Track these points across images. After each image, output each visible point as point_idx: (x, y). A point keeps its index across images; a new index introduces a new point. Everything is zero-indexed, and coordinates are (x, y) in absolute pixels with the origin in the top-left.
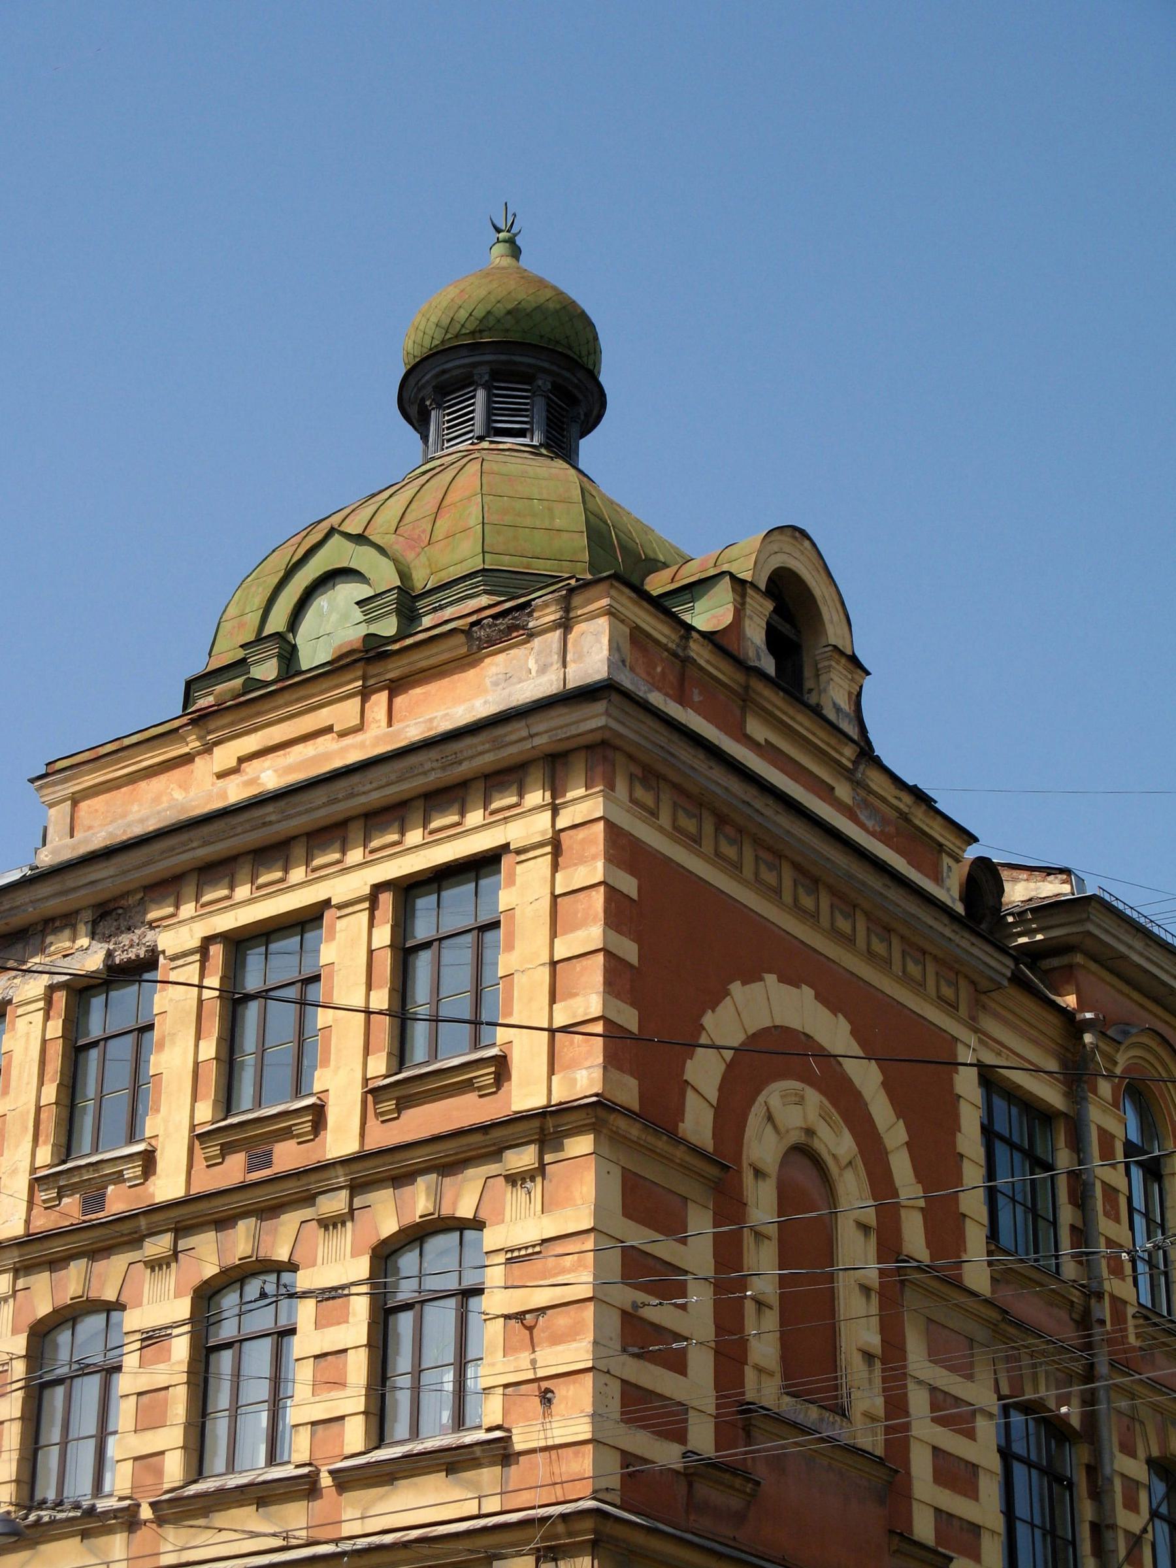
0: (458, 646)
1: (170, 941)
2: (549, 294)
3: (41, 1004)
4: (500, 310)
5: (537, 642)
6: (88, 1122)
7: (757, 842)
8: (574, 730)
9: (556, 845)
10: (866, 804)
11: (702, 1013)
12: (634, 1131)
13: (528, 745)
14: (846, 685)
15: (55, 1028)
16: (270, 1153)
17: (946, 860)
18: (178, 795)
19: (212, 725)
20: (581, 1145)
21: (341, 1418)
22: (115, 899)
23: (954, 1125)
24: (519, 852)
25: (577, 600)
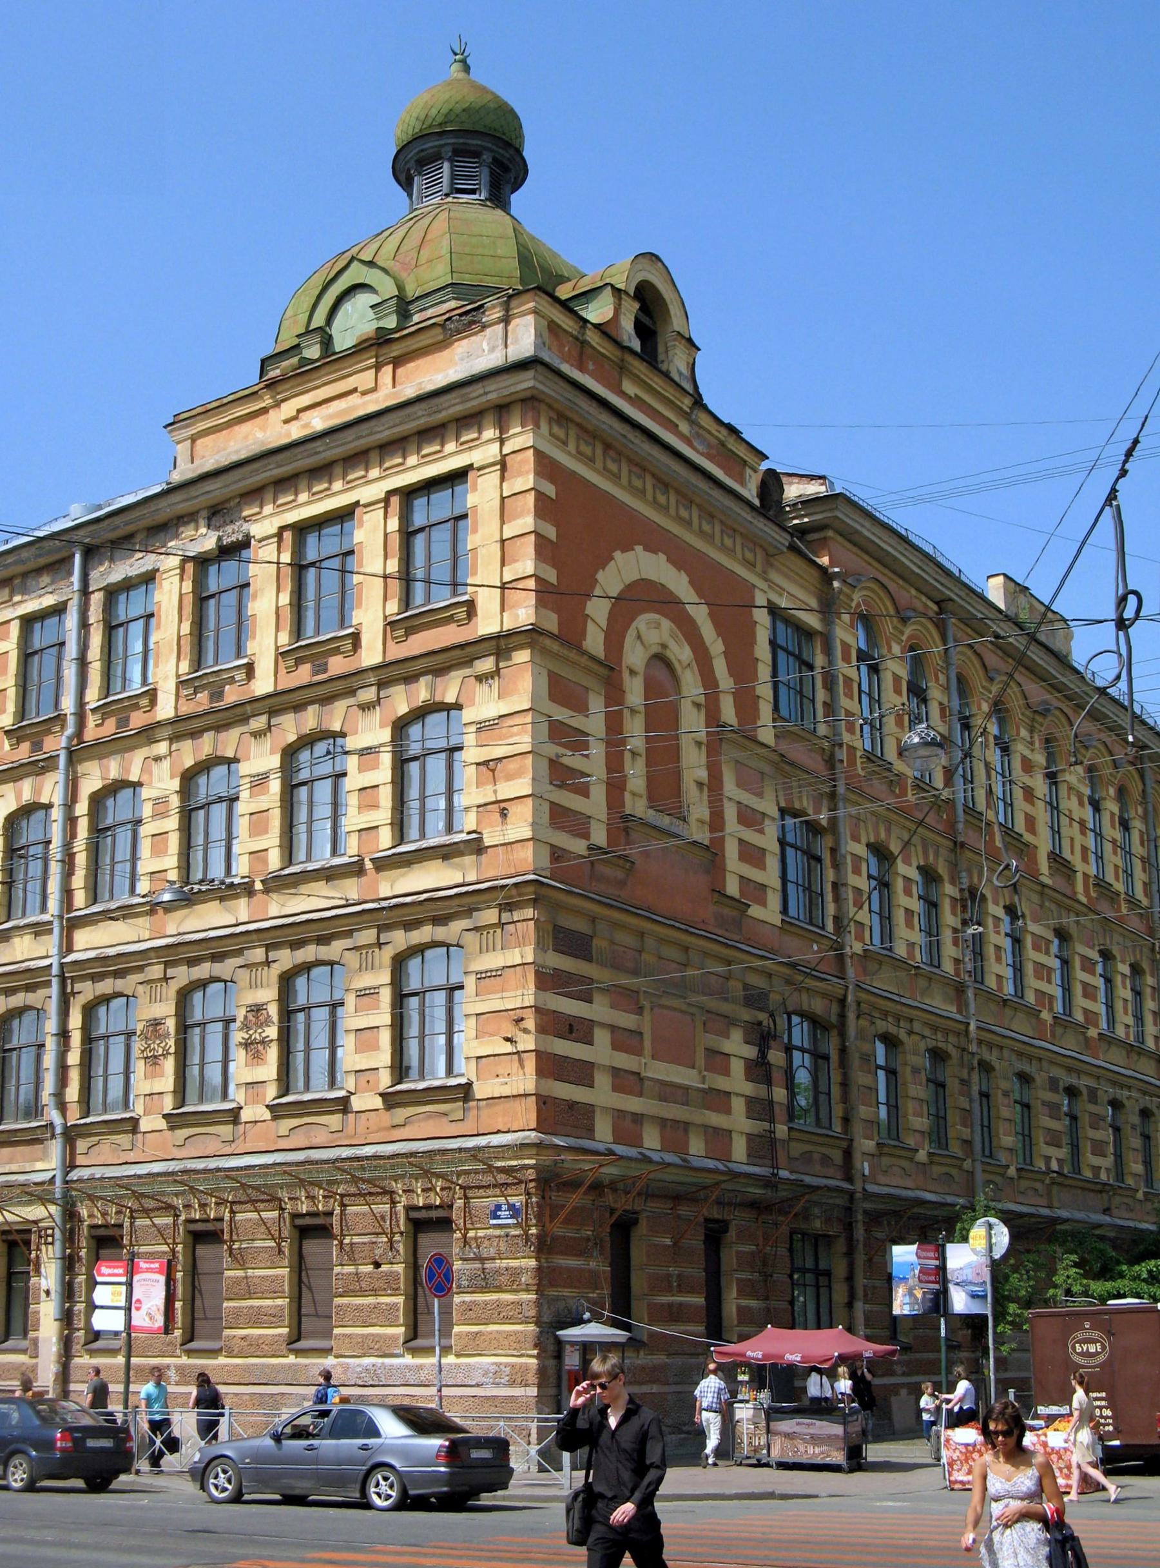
0: (437, 335)
1: (257, 530)
2: (489, 97)
3: (178, 571)
5: (488, 331)
6: (210, 645)
7: (630, 461)
8: (513, 389)
9: (503, 464)
10: (698, 435)
11: (596, 572)
12: (555, 646)
13: (484, 399)
14: (684, 357)
15: (188, 586)
16: (326, 664)
17: (748, 471)
18: (260, 435)
19: (280, 389)
20: (523, 656)
21: (377, 827)
22: (223, 503)
25: (514, 303)
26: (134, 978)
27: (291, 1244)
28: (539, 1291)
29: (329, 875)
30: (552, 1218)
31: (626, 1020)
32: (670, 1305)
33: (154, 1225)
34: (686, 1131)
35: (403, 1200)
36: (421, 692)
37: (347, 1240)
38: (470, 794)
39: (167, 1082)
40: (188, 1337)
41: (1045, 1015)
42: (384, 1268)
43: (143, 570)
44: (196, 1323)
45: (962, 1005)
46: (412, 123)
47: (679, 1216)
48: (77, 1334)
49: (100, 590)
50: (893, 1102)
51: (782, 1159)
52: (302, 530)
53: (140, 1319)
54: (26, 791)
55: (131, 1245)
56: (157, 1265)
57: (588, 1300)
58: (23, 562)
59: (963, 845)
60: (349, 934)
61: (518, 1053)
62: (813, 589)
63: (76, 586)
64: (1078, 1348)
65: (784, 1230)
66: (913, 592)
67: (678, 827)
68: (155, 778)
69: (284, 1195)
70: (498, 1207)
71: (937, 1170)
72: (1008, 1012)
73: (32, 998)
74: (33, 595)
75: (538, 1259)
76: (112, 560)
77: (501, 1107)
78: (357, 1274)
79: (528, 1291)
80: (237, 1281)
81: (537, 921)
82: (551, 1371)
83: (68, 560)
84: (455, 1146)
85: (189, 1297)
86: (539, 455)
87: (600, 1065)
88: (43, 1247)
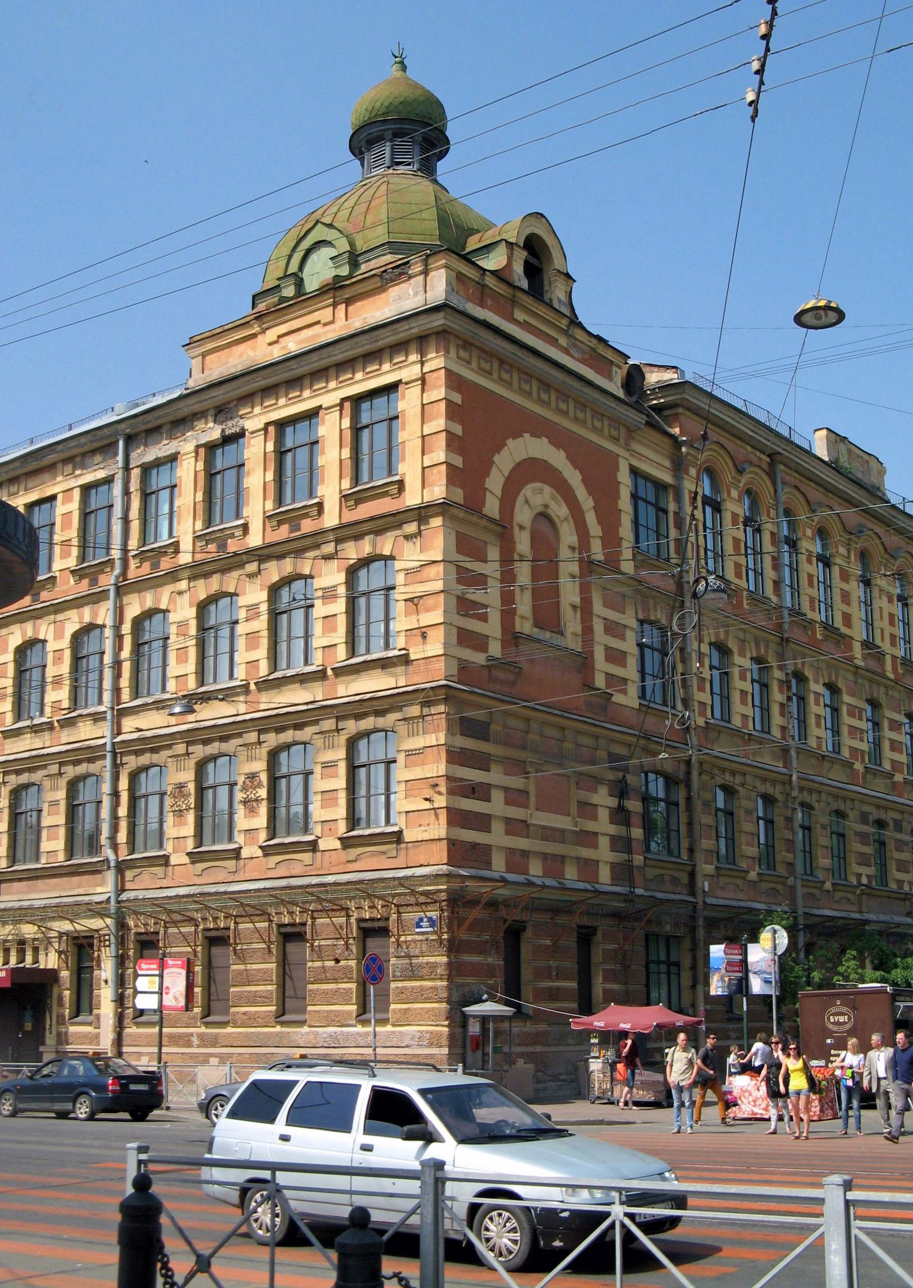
0: (377, 282)
1: (251, 424)
2: (420, 92)
3: (193, 454)
4: (396, 102)
5: (413, 280)
6: (218, 509)
7: (520, 371)
8: (429, 326)
9: (423, 380)
10: (575, 346)
11: (493, 455)
12: (461, 514)
13: (409, 333)
14: (564, 288)
15: (200, 466)
16: (299, 524)
17: (614, 369)
18: (251, 353)
19: (265, 320)
20: (437, 522)
21: (335, 645)
22: (224, 404)
23: (617, 496)
24: (407, 383)
25: (430, 261)
26: (165, 753)
27: (277, 946)
28: (450, 978)
29: (302, 679)
30: (459, 926)
31: (516, 782)
32: (550, 989)
33: (181, 933)
34: (563, 863)
35: (355, 915)
36: (366, 547)
37: (316, 944)
38: (401, 623)
39: (189, 829)
40: (206, 1013)
41: (858, 766)
42: (342, 963)
43: (168, 453)
44: (212, 1003)
45: (787, 763)
46: (363, 113)
47: (557, 924)
48: (128, 1011)
49: (137, 467)
50: (730, 836)
51: (638, 879)
52: (281, 425)
53: (168, 1001)
54: (88, 614)
55: (165, 947)
56: (180, 963)
57: (486, 985)
58: (82, 446)
59: (788, 640)
60: (316, 722)
61: (434, 809)
62: (666, 452)
63: (120, 464)
64: (832, 1020)
65: (641, 934)
66: (749, 448)
67: (558, 640)
68: (178, 607)
69: (272, 911)
70: (421, 920)
71: (765, 886)
72: (826, 765)
73: (93, 768)
74: (91, 469)
75: (448, 956)
76: (146, 445)
77: (423, 848)
78: (323, 967)
79: (441, 979)
80: (240, 973)
81: (448, 714)
82: (459, 1037)
83: (114, 444)
84: (391, 876)
85: (206, 984)
86: (449, 374)
87: (495, 816)
88: (103, 949)
